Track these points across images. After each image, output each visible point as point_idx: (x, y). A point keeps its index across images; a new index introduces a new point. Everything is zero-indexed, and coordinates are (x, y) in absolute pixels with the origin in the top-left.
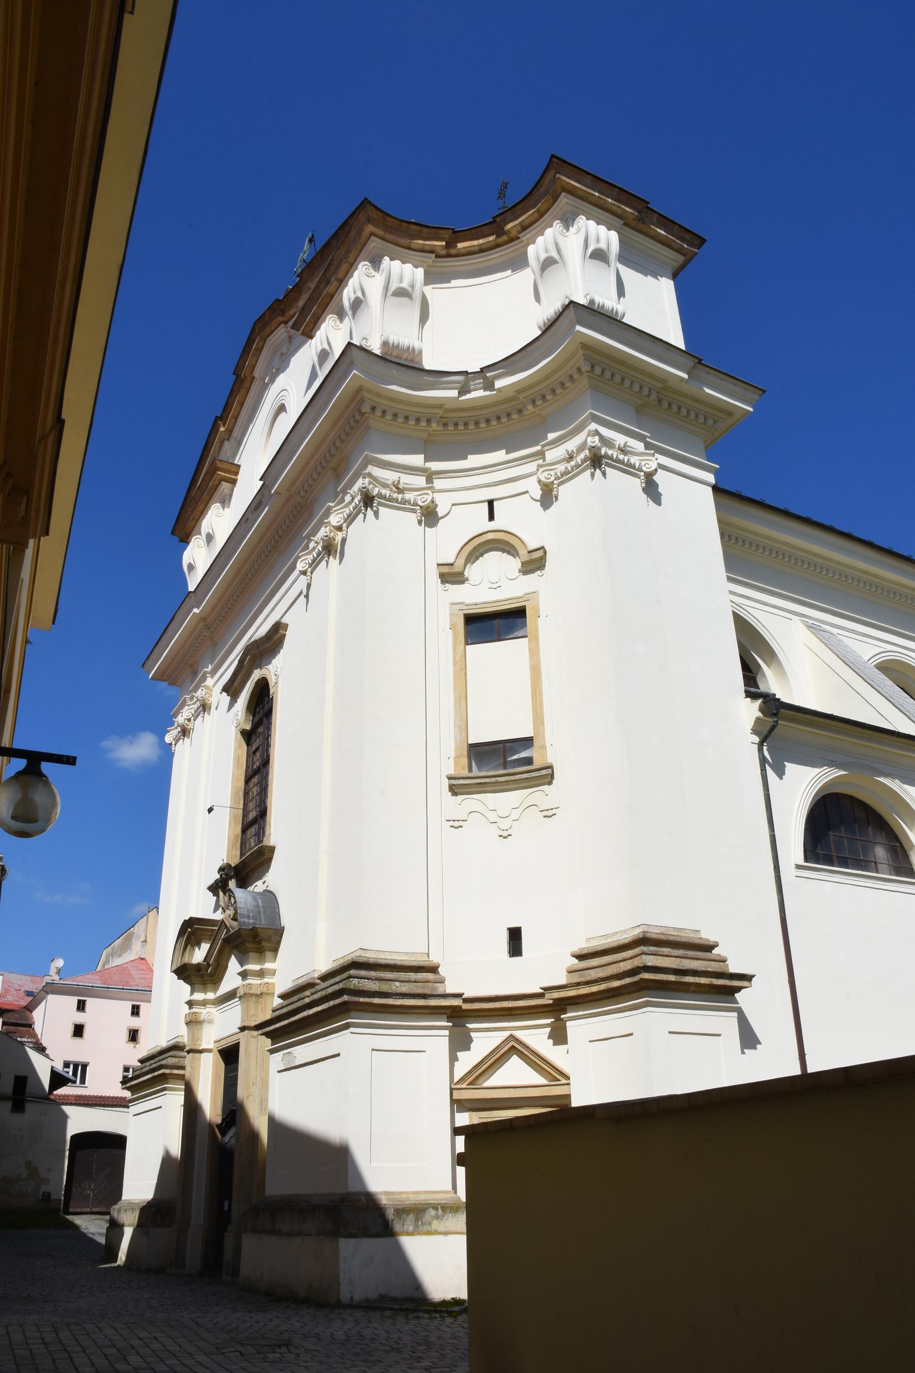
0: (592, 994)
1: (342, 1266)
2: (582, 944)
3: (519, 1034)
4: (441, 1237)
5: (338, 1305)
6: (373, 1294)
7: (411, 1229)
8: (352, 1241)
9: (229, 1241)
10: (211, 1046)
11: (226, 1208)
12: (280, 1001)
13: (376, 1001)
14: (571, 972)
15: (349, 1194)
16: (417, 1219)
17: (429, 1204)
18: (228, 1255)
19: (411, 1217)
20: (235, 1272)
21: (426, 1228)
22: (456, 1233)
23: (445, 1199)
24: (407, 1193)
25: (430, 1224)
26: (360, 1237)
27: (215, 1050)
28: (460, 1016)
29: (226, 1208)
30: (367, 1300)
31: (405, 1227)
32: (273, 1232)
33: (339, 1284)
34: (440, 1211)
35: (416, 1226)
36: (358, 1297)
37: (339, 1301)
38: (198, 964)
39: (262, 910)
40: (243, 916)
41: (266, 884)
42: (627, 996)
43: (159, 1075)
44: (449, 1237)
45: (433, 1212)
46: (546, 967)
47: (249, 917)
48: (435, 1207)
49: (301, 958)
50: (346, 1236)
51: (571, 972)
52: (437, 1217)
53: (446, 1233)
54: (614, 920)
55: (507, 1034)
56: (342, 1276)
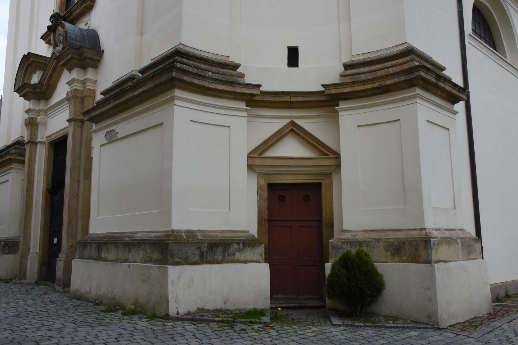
0: (365, 90)
1: (170, 288)
2: (346, 59)
3: (297, 121)
4: (243, 265)
5: (167, 317)
6: (193, 308)
7: (220, 258)
8: (178, 268)
9: (60, 264)
10: (44, 140)
11: (55, 241)
12: (102, 97)
13: (196, 82)
14: (341, 76)
15: (173, 231)
16: (224, 252)
17: (233, 240)
18: (59, 273)
19: (220, 249)
20: (67, 284)
21: (230, 258)
22: (253, 261)
23: (244, 237)
24: (215, 231)
25: (234, 255)
26: (183, 265)
27: (47, 143)
28: (258, 100)
29: (55, 241)
30: (189, 313)
31: (216, 257)
32: (99, 259)
33: (168, 302)
34: (241, 246)
35: (224, 256)
36: (182, 311)
37: (167, 315)
38: (35, 84)
39: (86, 38)
40: (72, 38)
41: (88, 25)
42: (395, 93)
43: (6, 160)
44: (249, 265)
45: (236, 246)
46: (317, 72)
47: (76, 40)
48: (238, 242)
49: (119, 63)
50: (173, 264)
51: (341, 76)
52: (239, 250)
53: (246, 262)
54: (373, 40)
55: (287, 121)
56: (170, 296)
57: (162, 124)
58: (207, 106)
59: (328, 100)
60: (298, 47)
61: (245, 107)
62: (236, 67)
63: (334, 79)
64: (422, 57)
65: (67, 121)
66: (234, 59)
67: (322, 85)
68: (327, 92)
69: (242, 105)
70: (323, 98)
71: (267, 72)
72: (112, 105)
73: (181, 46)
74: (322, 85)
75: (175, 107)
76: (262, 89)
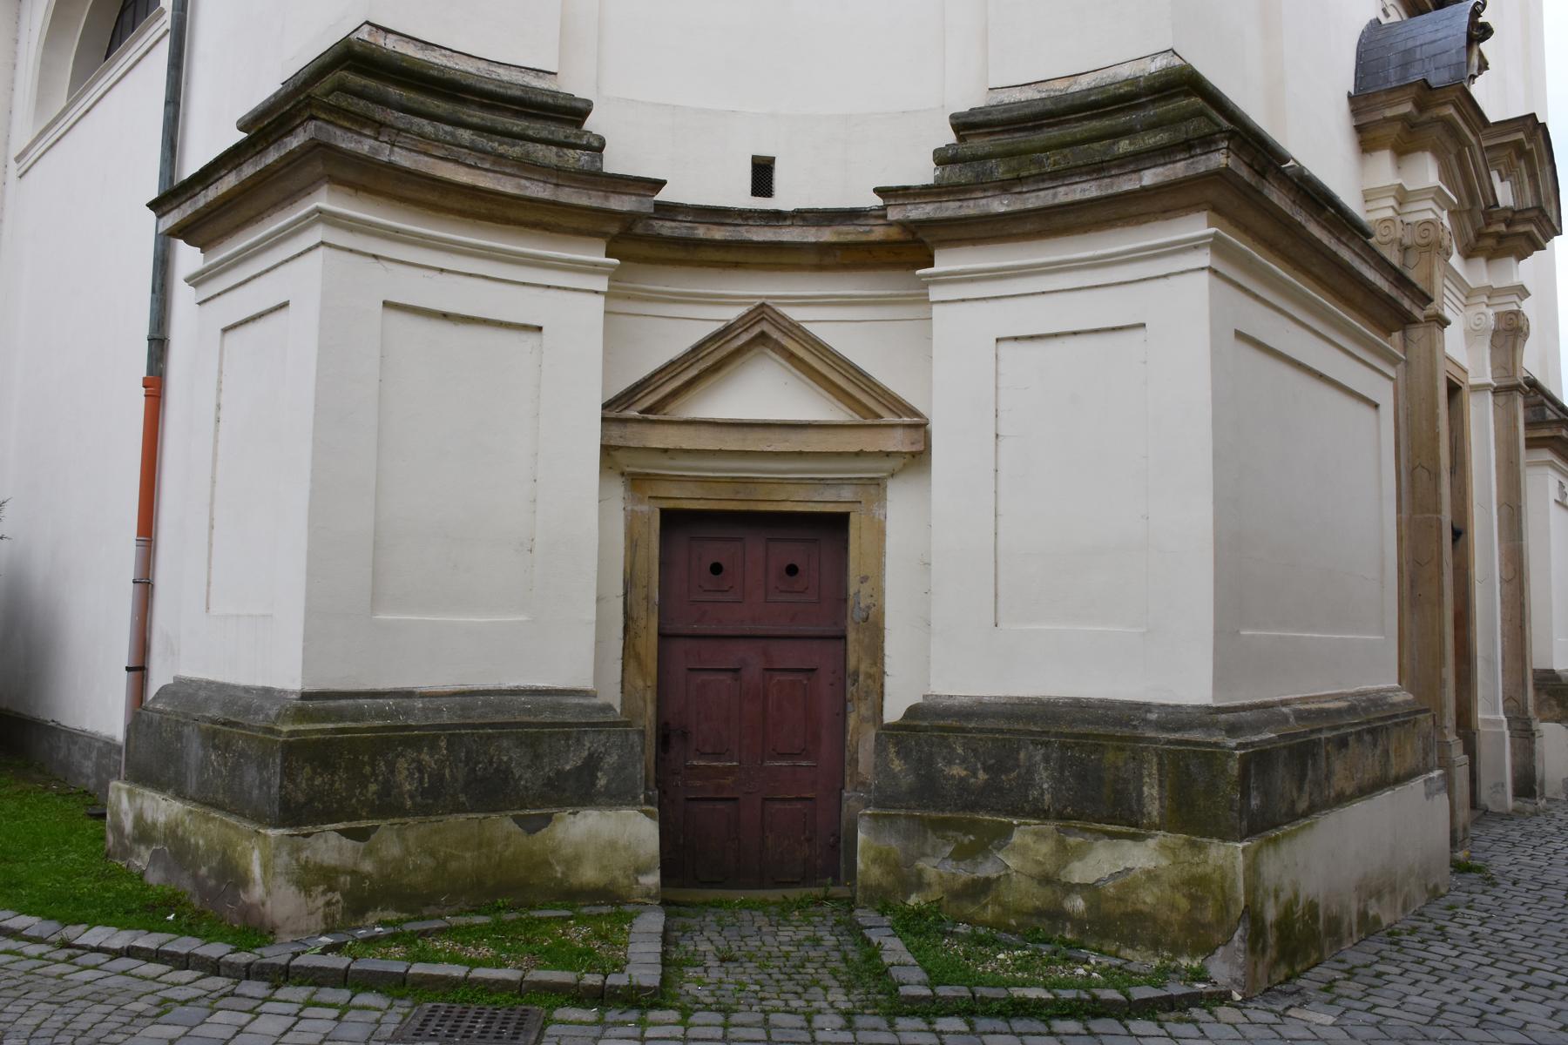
2: (969, 98)
28: (648, 236)
46: (865, 142)
57: (285, 305)
58: (972, 280)
59: (891, 244)
60: (589, 104)
61: (601, 258)
62: (576, 113)
63: (923, 172)
64: (1216, 100)
65: (153, 205)
66: (574, 85)
67: (877, 191)
68: (894, 214)
69: (595, 254)
70: (878, 233)
71: (672, 134)
72: (331, 726)
73: (364, 34)
74: (877, 191)
75: (935, 308)
76: (663, 196)
